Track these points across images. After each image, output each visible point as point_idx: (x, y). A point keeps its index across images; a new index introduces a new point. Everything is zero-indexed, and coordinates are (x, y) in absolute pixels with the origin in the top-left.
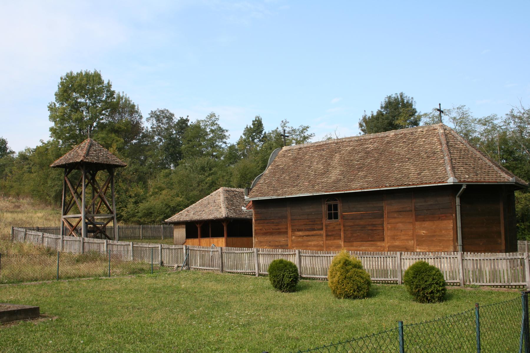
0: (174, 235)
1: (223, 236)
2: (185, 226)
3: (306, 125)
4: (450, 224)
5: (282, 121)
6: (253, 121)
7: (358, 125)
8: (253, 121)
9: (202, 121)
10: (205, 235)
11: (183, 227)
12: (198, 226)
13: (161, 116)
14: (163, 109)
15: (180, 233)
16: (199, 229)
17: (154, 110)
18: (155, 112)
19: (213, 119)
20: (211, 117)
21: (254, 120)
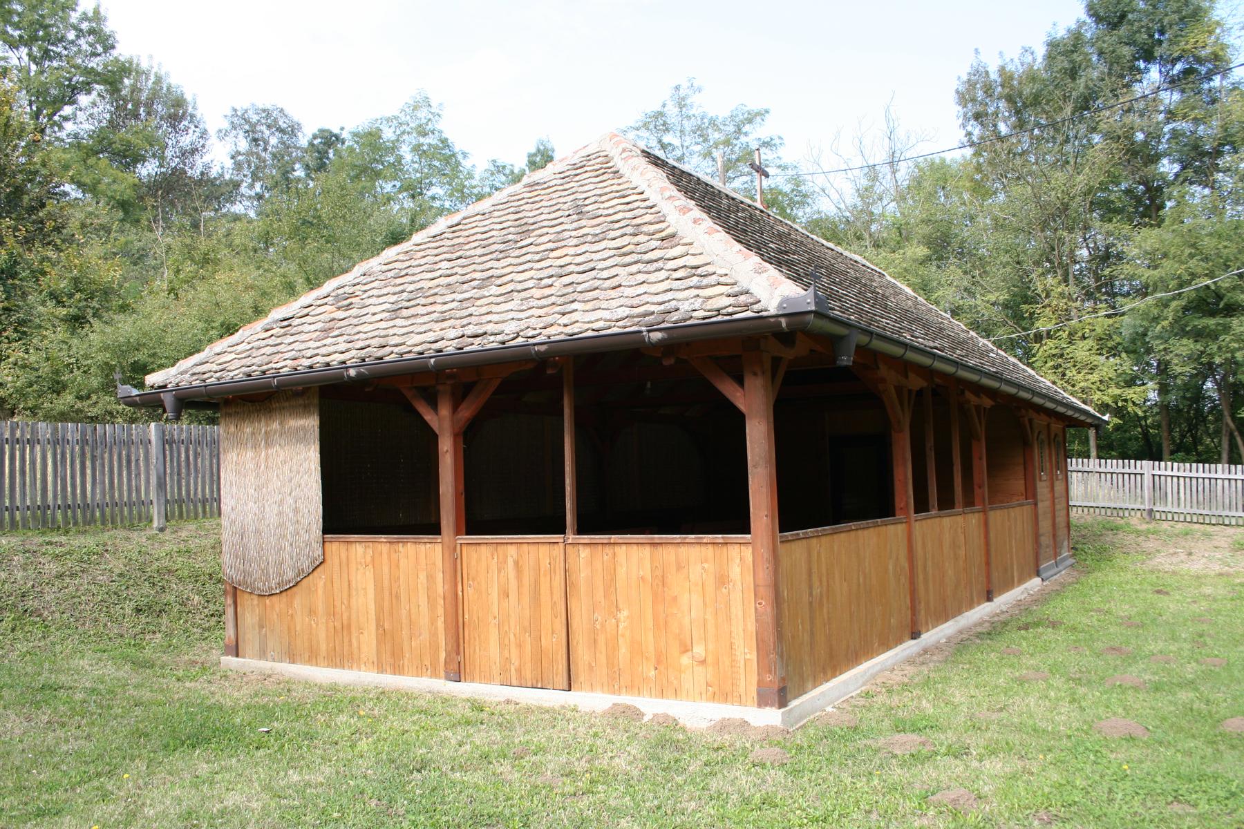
0: (227, 503)
1: (733, 519)
2: (312, 423)
3: (755, 106)
4: (438, 548)
5: (677, 88)
6: (530, 156)
7: (953, 97)
8: (530, 156)
9: (388, 120)
10: (510, 505)
11: (299, 437)
12: (443, 422)
13: (254, 126)
14: (268, 106)
15: (274, 480)
16: (446, 446)
17: (241, 105)
18: (246, 111)
19: (423, 114)
20: (415, 108)
21: (533, 150)
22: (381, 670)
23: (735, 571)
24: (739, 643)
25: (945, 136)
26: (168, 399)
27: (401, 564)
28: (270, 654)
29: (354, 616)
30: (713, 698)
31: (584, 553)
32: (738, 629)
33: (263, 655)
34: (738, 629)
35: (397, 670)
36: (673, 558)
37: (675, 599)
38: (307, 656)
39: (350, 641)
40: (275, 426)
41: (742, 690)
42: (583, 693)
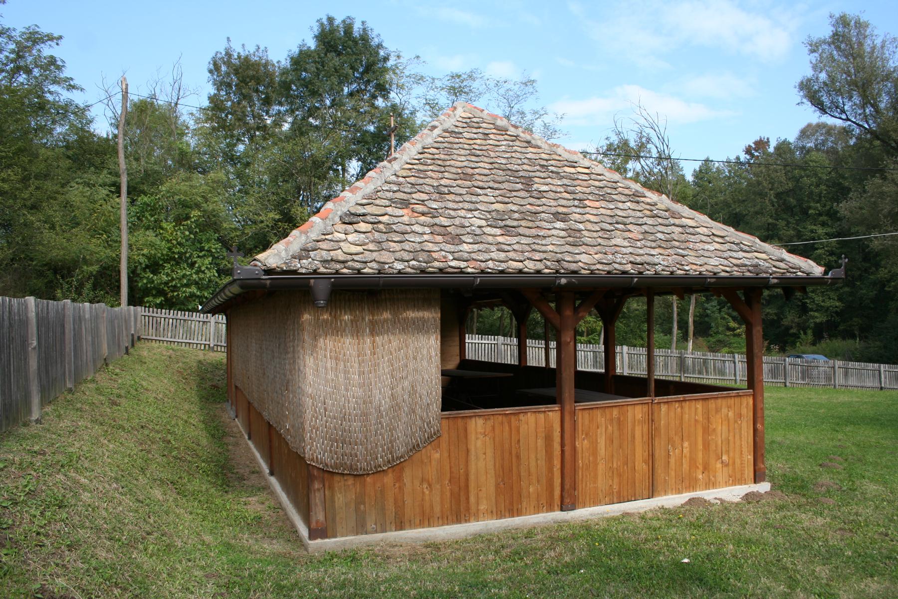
3: (45, 29)
11: (420, 327)
22: (500, 516)
23: (744, 411)
24: (745, 450)
25: (193, 96)
26: (322, 289)
27: (521, 430)
28: (371, 525)
29: (472, 477)
30: (734, 483)
31: (664, 408)
32: (744, 444)
33: (360, 528)
34: (744, 444)
35: (514, 511)
36: (714, 406)
37: (714, 430)
38: (417, 521)
39: (468, 499)
40: (386, 315)
41: (746, 476)
42: (660, 498)
